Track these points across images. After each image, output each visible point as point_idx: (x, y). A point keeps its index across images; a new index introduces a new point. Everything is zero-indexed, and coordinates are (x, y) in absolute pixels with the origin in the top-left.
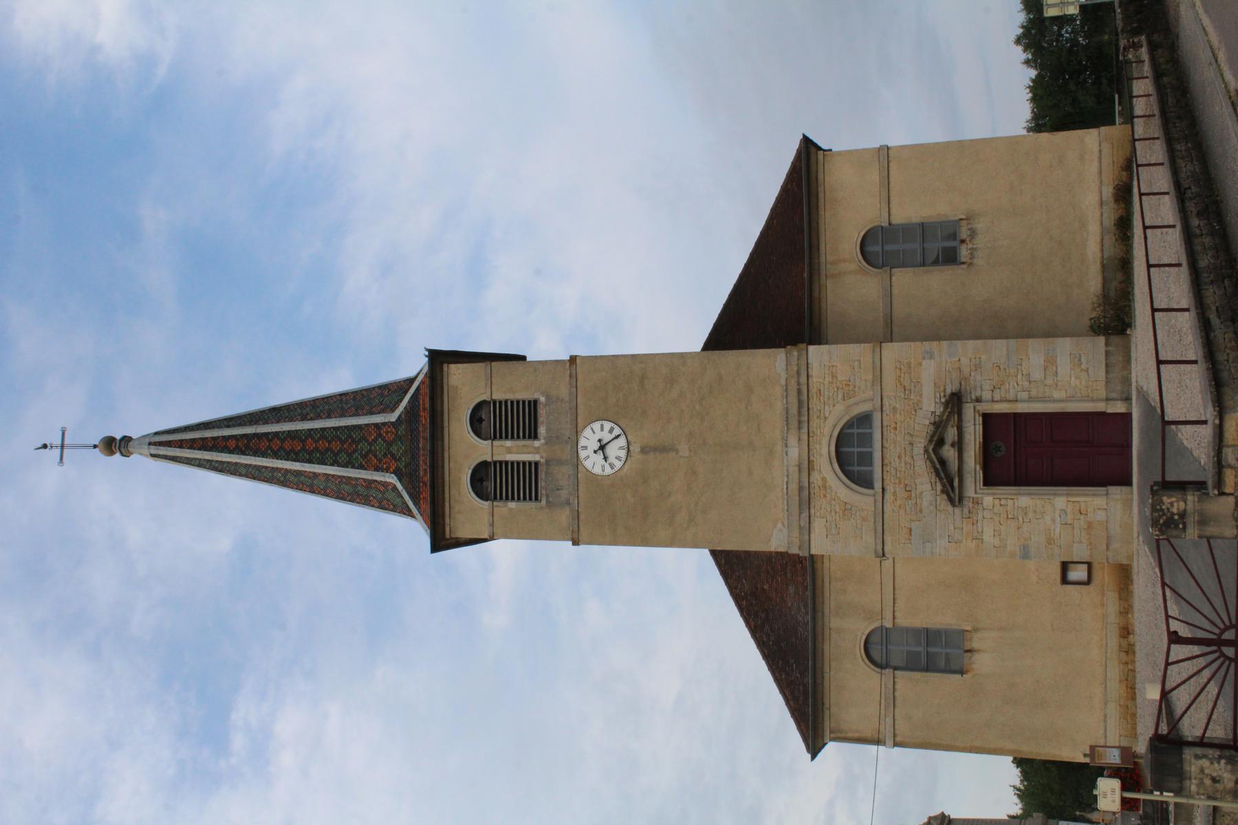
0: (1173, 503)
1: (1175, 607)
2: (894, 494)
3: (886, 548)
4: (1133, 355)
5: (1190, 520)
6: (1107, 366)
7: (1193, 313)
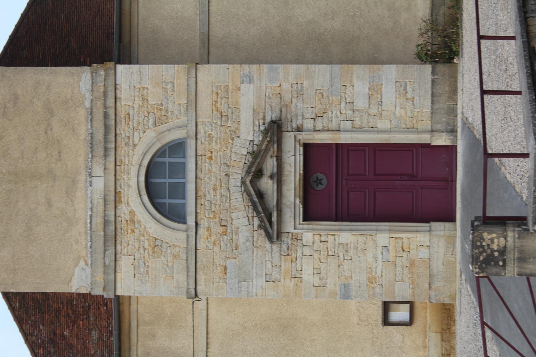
0: (494, 239)
1: (495, 348)
2: (209, 229)
3: (199, 288)
4: (460, 85)
5: (510, 257)
6: (433, 95)
7: (519, 41)
